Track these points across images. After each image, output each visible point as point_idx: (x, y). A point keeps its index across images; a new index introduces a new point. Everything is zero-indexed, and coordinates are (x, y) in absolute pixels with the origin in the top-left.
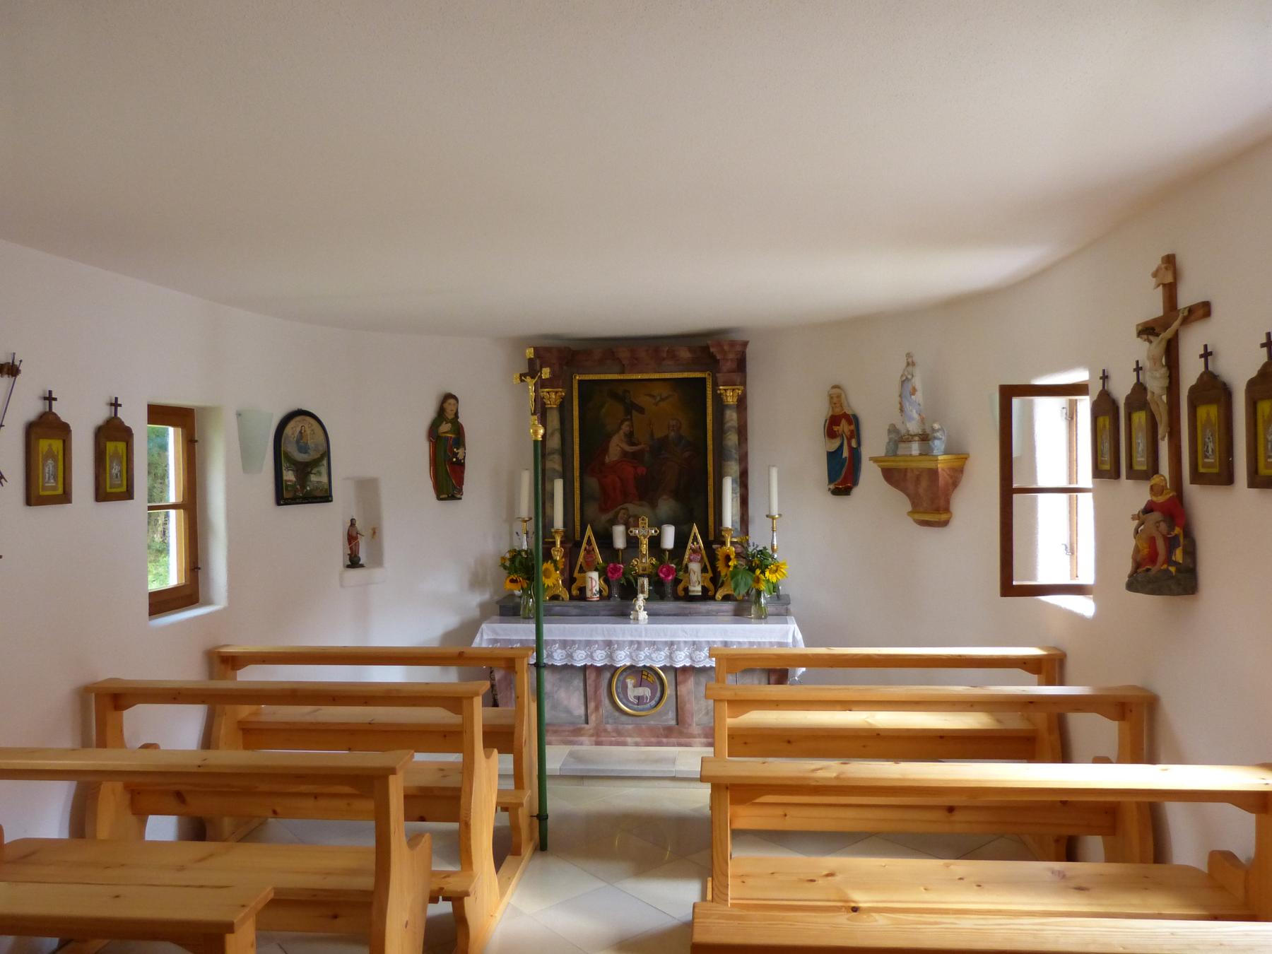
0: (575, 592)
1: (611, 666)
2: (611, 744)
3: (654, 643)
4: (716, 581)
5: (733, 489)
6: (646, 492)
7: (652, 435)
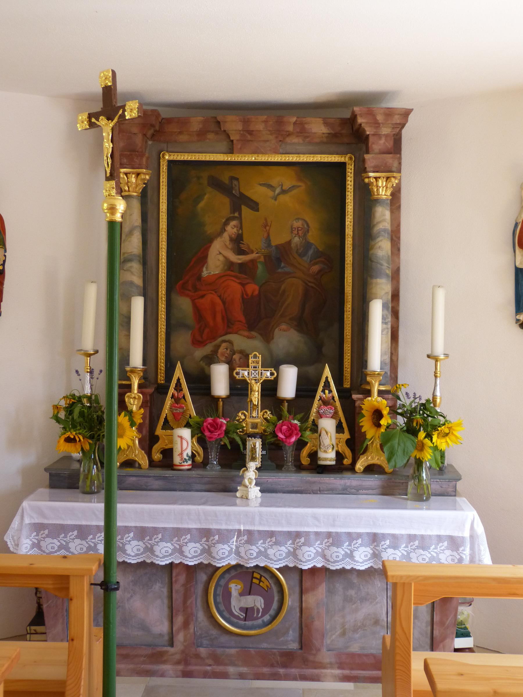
0: (157, 456)
1: (209, 565)
2: (206, 675)
3: (272, 534)
4: (356, 443)
5: (384, 318)
6: (259, 318)
7: (268, 239)
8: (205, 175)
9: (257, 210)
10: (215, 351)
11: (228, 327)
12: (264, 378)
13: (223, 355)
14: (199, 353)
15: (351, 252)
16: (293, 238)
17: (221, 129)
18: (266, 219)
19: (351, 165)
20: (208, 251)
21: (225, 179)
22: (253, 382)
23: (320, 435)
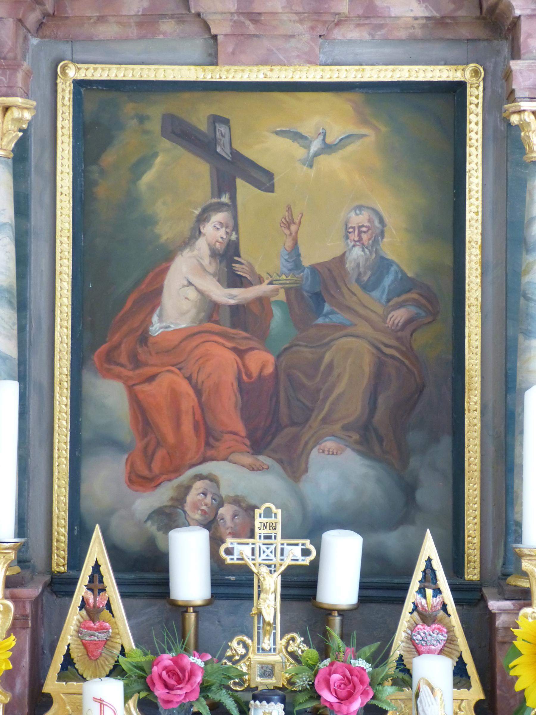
6: (275, 424)
8: (156, 110)
9: (271, 189)
10: (179, 500)
11: (208, 444)
12: (288, 562)
13: (196, 506)
14: (146, 502)
15: (479, 280)
16: (350, 250)
17: (189, 10)
18: (289, 209)
19: (477, 88)
20: (163, 280)
21: (200, 120)
22: (264, 570)
23: (417, 695)
